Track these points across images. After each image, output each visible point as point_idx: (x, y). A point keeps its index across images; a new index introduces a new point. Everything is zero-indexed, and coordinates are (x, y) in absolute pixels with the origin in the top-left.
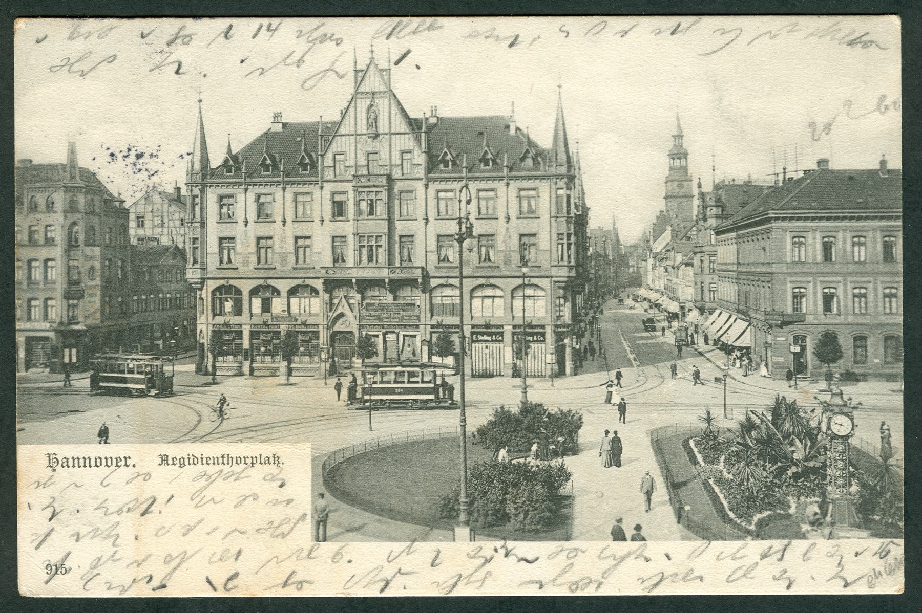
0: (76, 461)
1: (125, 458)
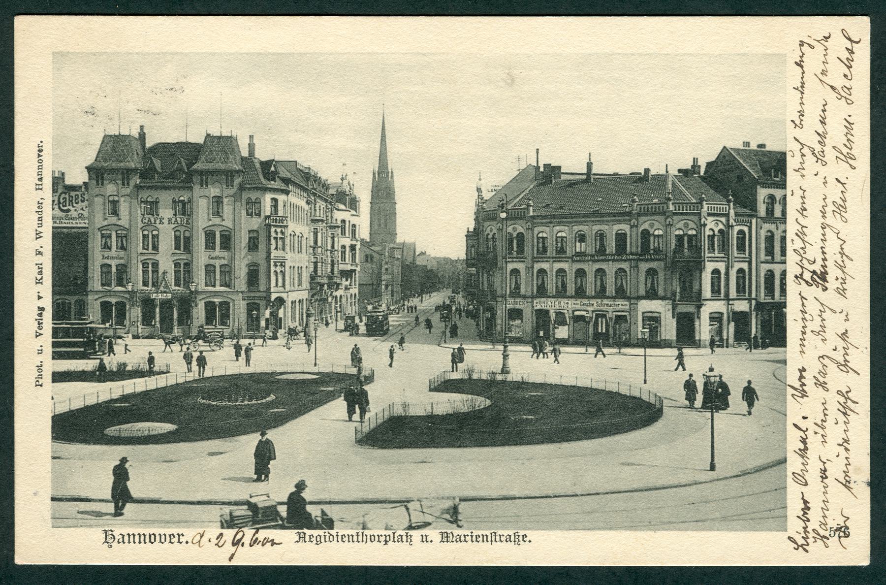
0: (142, 537)
1: (178, 535)
